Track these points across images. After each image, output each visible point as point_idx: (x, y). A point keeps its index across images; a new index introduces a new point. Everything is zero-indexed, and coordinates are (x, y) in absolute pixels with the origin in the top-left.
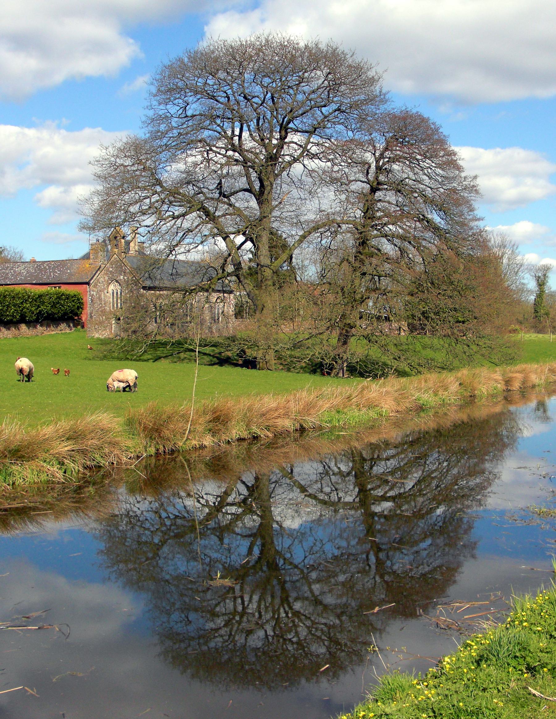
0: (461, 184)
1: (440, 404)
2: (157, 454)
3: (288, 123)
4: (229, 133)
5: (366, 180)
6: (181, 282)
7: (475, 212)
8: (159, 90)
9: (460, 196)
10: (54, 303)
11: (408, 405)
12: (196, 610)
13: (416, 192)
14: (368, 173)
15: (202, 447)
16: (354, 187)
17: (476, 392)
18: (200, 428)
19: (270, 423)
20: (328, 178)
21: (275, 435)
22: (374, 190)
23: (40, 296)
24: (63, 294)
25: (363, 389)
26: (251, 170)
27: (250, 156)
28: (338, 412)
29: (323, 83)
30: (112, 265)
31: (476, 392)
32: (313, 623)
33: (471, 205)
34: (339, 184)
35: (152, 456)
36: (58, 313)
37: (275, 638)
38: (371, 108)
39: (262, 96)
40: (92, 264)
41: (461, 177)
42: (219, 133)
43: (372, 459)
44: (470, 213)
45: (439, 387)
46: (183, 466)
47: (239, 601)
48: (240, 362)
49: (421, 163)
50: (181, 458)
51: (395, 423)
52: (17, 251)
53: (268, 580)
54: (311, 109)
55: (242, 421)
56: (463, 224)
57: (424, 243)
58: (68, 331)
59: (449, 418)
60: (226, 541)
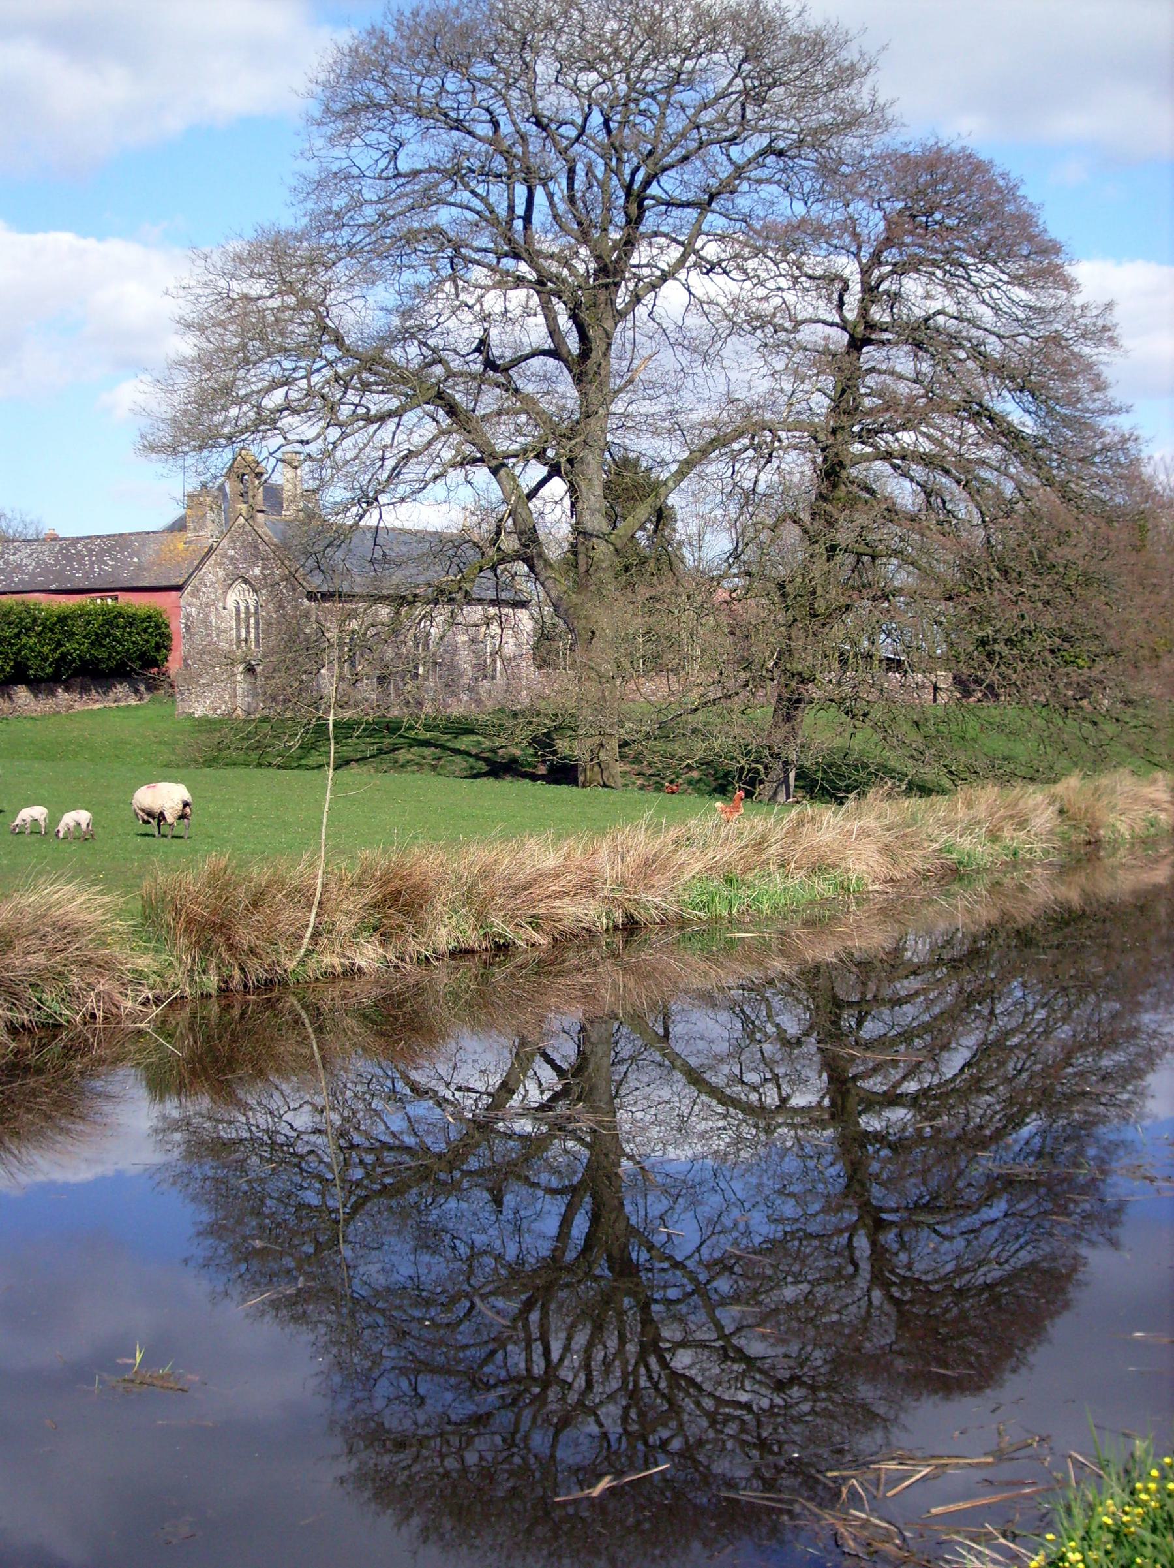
0: (1073, 325)
1: (1003, 863)
2: (225, 991)
3: (647, 184)
4: (503, 211)
5: (837, 320)
6: (395, 580)
7: (1110, 393)
8: (327, 109)
9: (1072, 352)
10: (97, 634)
11: (918, 865)
12: (433, 1370)
13: (961, 346)
14: (841, 304)
15: (352, 973)
16: (811, 335)
17: (1102, 832)
18: (346, 924)
19: (541, 910)
20: (742, 315)
21: (555, 940)
22: (856, 344)
23: (63, 619)
24: (120, 615)
25: (801, 823)
26: (554, 300)
27: (554, 267)
28: (729, 881)
29: (730, 84)
30: (234, 541)
31: (1102, 832)
32: (719, 1401)
33: (1099, 375)
34: (769, 329)
35: (209, 996)
36: (109, 659)
37: (624, 1439)
38: (851, 142)
39: (579, 121)
40: (190, 542)
41: (1074, 308)
42: (478, 213)
43: (863, 1000)
44: (1096, 395)
45: (1003, 818)
46: (297, 1021)
47: (538, 1347)
48: (542, 770)
49: (973, 273)
50: (292, 1000)
51: (882, 911)
52: (28, 520)
53: (607, 1300)
54: (700, 148)
55: (464, 906)
56: (1076, 424)
57: (985, 473)
58: (134, 703)
59: (1030, 898)
60: (509, 1200)
